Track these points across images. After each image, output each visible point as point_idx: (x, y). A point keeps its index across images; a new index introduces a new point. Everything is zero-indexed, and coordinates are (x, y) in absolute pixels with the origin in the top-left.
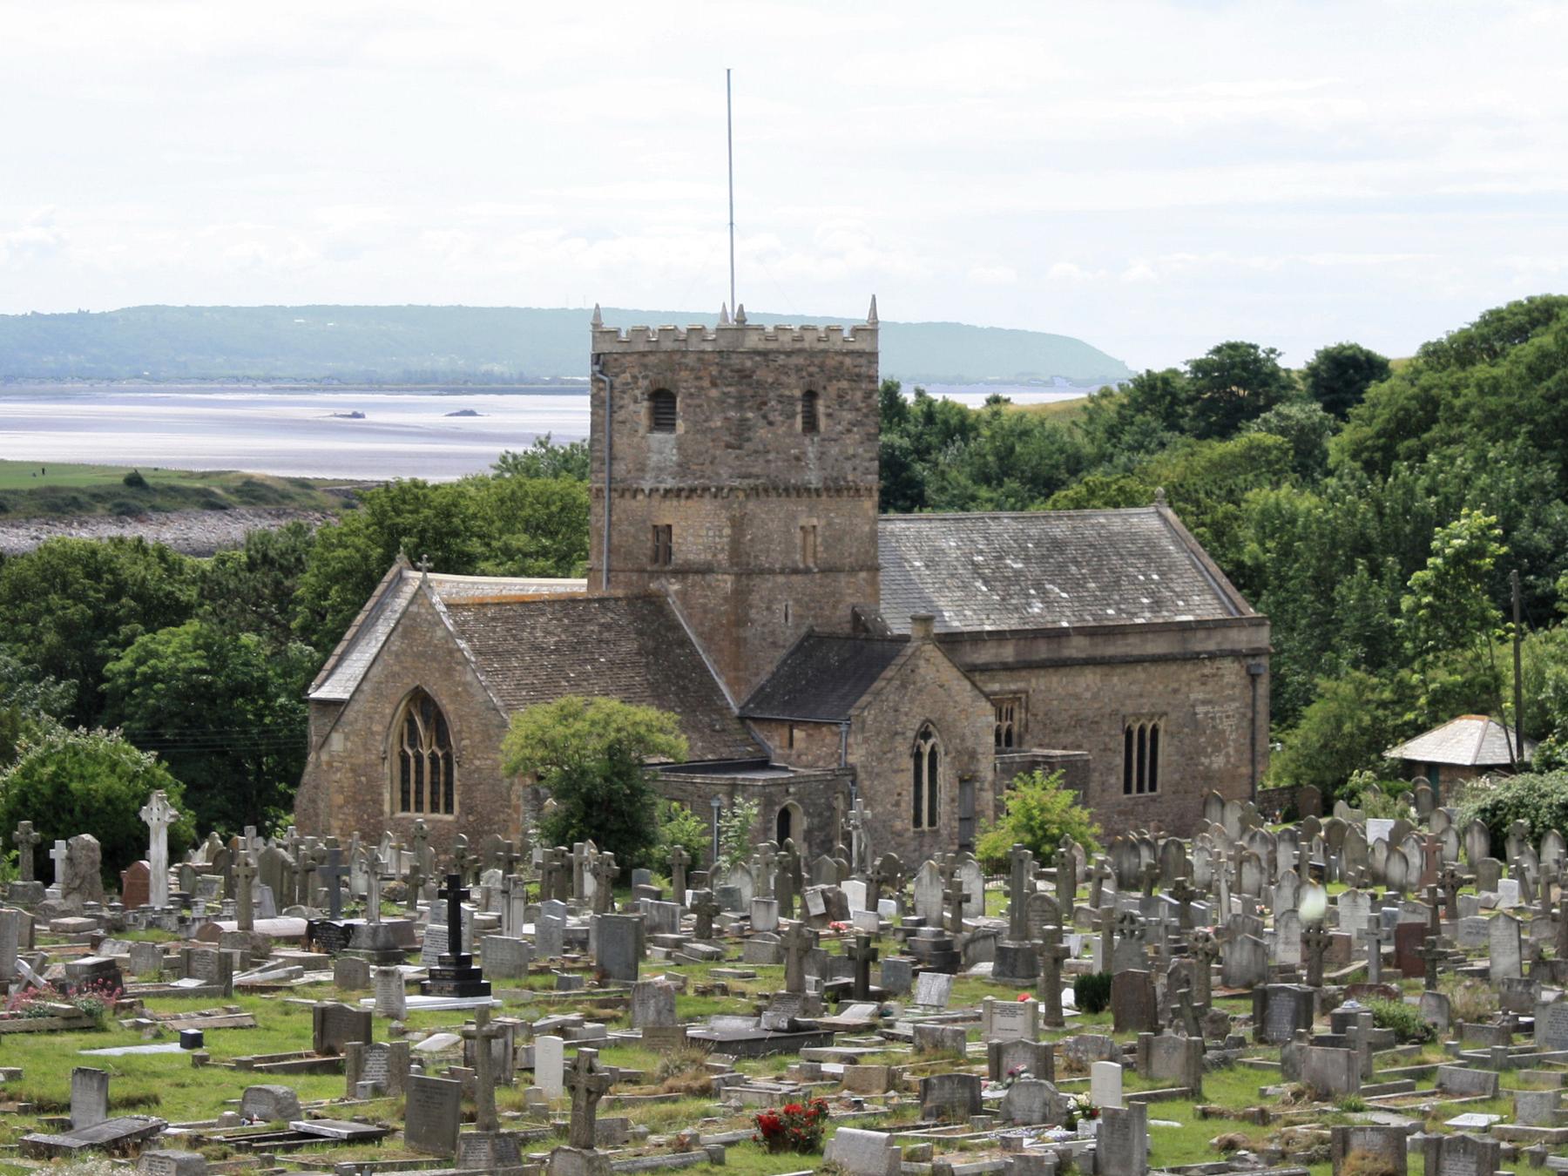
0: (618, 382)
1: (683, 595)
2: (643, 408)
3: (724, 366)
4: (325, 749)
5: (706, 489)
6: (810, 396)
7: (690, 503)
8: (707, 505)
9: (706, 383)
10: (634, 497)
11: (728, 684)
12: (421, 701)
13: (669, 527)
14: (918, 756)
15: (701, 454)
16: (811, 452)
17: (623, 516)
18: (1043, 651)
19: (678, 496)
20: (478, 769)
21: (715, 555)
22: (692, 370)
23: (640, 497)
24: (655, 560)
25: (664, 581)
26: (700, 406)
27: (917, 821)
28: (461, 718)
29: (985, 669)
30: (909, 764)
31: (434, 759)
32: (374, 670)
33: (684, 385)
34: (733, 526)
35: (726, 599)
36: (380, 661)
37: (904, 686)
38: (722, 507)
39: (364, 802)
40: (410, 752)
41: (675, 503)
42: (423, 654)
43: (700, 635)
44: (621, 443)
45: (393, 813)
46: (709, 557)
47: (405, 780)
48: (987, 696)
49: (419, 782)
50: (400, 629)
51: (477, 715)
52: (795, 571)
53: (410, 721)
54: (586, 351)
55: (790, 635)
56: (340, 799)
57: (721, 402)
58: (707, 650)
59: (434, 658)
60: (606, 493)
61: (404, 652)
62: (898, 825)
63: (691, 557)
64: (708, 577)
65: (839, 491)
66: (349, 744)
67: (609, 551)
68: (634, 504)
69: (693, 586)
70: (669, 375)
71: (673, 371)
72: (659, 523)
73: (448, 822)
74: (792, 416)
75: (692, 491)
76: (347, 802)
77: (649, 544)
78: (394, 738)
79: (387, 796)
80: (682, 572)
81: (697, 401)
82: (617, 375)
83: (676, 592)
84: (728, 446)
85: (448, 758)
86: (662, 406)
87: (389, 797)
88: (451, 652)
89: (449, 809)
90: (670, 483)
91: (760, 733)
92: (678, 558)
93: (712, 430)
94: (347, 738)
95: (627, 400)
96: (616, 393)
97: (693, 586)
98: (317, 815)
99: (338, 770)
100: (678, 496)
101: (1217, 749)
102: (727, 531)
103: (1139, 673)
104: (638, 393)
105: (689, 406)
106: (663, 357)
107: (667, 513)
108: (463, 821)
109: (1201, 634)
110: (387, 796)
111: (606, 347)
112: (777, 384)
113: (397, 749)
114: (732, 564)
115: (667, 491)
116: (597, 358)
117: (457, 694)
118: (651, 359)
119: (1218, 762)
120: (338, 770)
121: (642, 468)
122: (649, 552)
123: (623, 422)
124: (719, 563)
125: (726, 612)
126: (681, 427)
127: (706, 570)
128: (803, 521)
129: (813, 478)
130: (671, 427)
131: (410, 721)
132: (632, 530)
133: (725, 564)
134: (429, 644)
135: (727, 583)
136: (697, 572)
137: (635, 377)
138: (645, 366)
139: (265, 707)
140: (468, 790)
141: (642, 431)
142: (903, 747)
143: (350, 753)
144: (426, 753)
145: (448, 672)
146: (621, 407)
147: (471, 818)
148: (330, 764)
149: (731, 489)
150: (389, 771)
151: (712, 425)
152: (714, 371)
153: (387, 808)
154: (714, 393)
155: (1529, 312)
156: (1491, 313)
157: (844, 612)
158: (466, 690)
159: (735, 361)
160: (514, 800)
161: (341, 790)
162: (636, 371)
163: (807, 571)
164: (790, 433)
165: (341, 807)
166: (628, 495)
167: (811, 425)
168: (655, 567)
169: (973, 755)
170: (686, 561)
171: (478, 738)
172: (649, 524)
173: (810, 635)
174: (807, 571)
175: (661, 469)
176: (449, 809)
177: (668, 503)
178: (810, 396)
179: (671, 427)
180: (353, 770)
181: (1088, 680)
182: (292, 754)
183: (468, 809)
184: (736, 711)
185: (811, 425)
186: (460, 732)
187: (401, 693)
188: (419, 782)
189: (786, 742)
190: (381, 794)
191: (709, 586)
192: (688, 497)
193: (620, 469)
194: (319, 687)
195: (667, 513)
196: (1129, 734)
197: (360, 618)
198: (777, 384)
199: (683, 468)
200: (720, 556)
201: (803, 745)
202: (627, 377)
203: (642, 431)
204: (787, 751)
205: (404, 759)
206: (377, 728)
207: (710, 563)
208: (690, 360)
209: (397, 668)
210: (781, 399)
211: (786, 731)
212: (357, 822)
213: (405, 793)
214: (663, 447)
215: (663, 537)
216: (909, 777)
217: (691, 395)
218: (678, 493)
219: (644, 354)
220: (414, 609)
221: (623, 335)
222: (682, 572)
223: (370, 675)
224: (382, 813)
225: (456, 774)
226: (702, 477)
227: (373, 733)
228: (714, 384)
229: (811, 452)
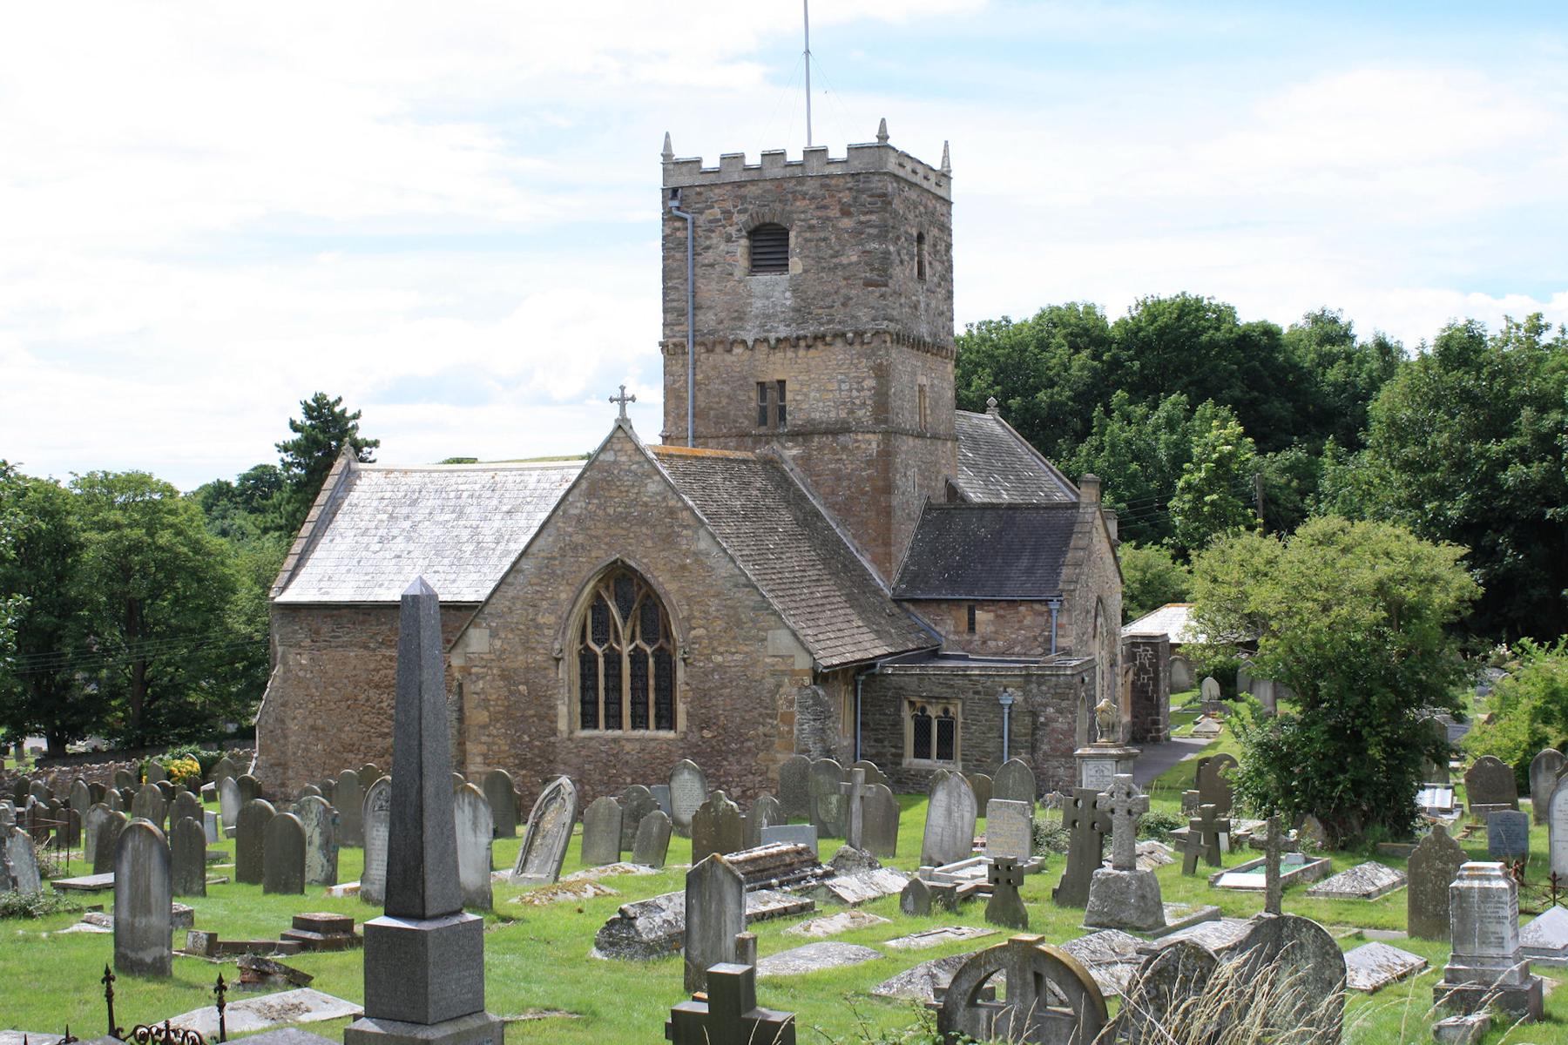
0: (701, 220)
1: (805, 461)
2: (741, 247)
3: (863, 191)
4: (459, 650)
7: (812, 352)
8: (839, 352)
9: (834, 212)
10: (729, 351)
11: (873, 561)
12: (622, 580)
13: (782, 384)
15: (828, 295)
17: (712, 373)
19: (796, 346)
20: (719, 667)
21: (851, 412)
22: (813, 198)
23: (738, 350)
24: (763, 420)
25: (776, 446)
26: (824, 240)
28: (689, 600)
31: (638, 658)
32: (540, 542)
34: (877, 377)
35: (870, 463)
36: (551, 529)
38: (860, 356)
39: (524, 719)
40: (599, 650)
41: (790, 354)
42: (625, 518)
43: (831, 506)
44: (710, 290)
45: (571, 732)
46: (843, 415)
50: (584, 485)
51: (717, 595)
54: (655, 179)
56: (483, 717)
57: (856, 233)
58: (843, 523)
59: (643, 522)
60: (689, 348)
61: (592, 516)
63: (816, 415)
64: (841, 438)
66: (498, 643)
67: (694, 415)
68: (729, 358)
69: (820, 449)
70: (778, 206)
71: (784, 201)
72: (766, 379)
73: (667, 741)
75: (819, 338)
76: (494, 719)
77: (753, 404)
78: (573, 633)
79: (562, 710)
80: (802, 434)
81: (822, 235)
82: (701, 212)
83: (794, 458)
84: (868, 283)
86: (768, 245)
87: (565, 711)
88: (672, 512)
89: (666, 719)
90: (783, 332)
91: (923, 617)
92: (795, 418)
93: (844, 267)
94: (494, 634)
95: (715, 239)
96: (700, 232)
97: (820, 449)
98: (285, 737)
99: (479, 677)
100: (796, 346)
102: (870, 383)
104: (732, 230)
105: (807, 240)
106: (769, 186)
107: (776, 367)
108: (694, 737)
111: (684, 180)
113: (577, 646)
114: (877, 421)
115: (778, 340)
116: (671, 193)
117: (684, 567)
118: (751, 190)
120: (479, 677)
121: (741, 317)
122: (755, 414)
123: (712, 266)
124: (859, 421)
125: (870, 478)
126: (796, 265)
127: (838, 430)
130: (783, 266)
131: (598, 607)
132: (727, 388)
133: (868, 421)
134: (634, 503)
136: (826, 433)
137: (727, 214)
138: (743, 198)
140: (702, 696)
141: (738, 274)
143: (500, 655)
144: (626, 649)
145: (669, 540)
146: (708, 248)
147: (707, 734)
148: (466, 670)
149: (877, 333)
150: (568, 674)
151: (845, 261)
152: (846, 197)
153: (562, 725)
154: (846, 223)
156: (138, 482)
158: (702, 565)
159: (876, 183)
160: (782, 706)
161: (485, 703)
162: (729, 205)
165: (484, 727)
166: (719, 349)
168: (763, 430)
170: (810, 421)
171: (719, 625)
172: (752, 381)
175: (768, 317)
176: (666, 719)
177: (780, 355)
179: (783, 266)
180: (503, 677)
182: (248, 668)
183: (701, 721)
184: (888, 593)
186: (688, 619)
187: (586, 572)
189: (964, 625)
190: (553, 707)
191: (844, 448)
192: (808, 347)
194: (283, 589)
197: (314, 513)
199: (801, 313)
200: (860, 413)
201: (991, 628)
203: (738, 274)
204: (966, 637)
205: (587, 659)
206: (546, 619)
207: (844, 421)
208: (811, 187)
209: (579, 539)
211: (964, 614)
212: (513, 745)
214: (772, 292)
215: (772, 395)
217: (811, 228)
218: (794, 343)
219: (740, 185)
220: (608, 457)
221: (706, 165)
222: (802, 434)
223: (534, 549)
224: (554, 732)
225: (681, 674)
226: (829, 322)
227: (538, 627)
228: (846, 213)
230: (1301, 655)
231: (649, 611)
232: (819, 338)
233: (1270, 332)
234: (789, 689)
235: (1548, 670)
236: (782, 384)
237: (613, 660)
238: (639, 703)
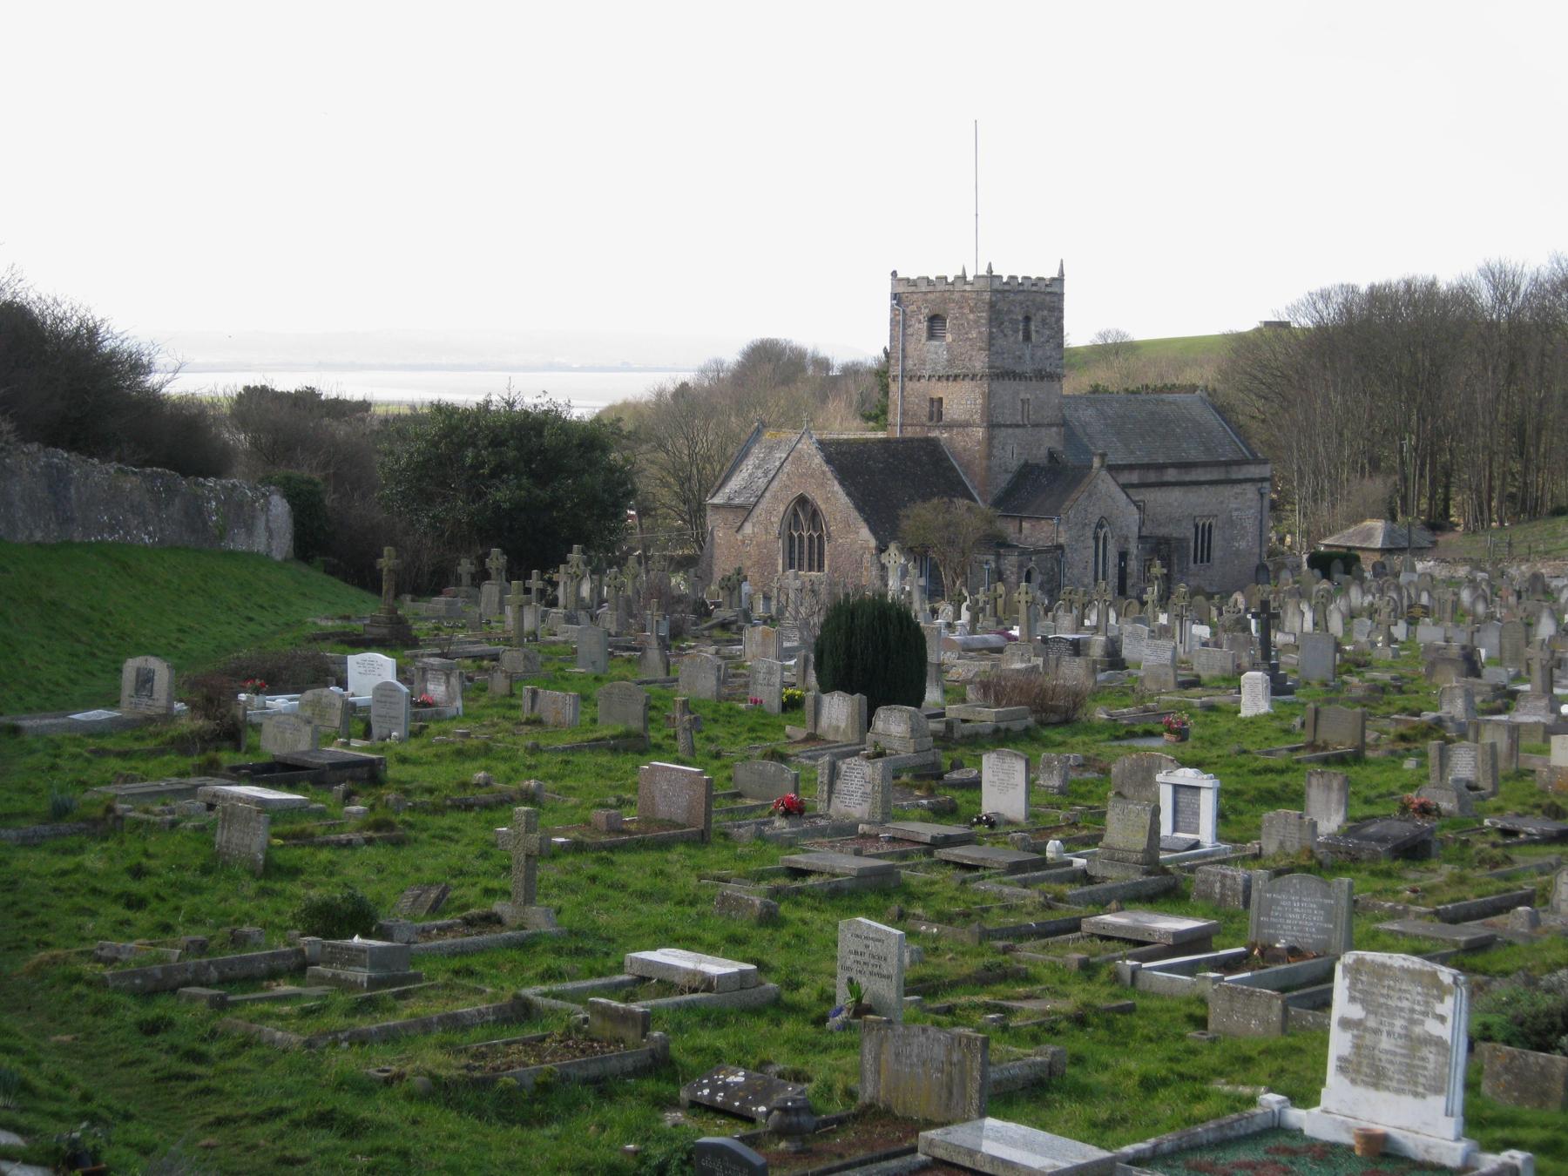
5: (965, 376)
6: (1027, 319)
9: (966, 311)
12: (802, 501)
13: (941, 400)
14: (1096, 539)
16: (1028, 353)
18: (1152, 477)
20: (842, 545)
24: (931, 419)
27: (1096, 580)
29: (1133, 486)
30: (1092, 543)
31: (811, 538)
33: (952, 311)
37: (1090, 495)
47: (791, 552)
48: (1135, 503)
49: (801, 553)
52: (1018, 426)
53: (796, 515)
55: (1014, 464)
57: (976, 322)
62: (1086, 581)
65: (1042, 378)
74: (1017, 331)
75: (956, 377)
80: (950, 426)
85: (820, 537)
89: (821, 568)
92: (946, 418)
101: (1243, 537)
103: (1203, 490)
107: (938, 390)
109: (1235, 468)
110: (780, 561)
111: (900, 290)
112: (1009, 312)
119: (1243, 545)
126: (949, 338)
127: (966, 425)
128: (1022, 396)
129: (1028, 367)
135: (979, 433)
139: (1476, 619)
142: (1089, 533)
154: (971, 316)
155: (497, 442)
157: (1043, 452)
163: (1024, 426)
164: (1016, 342)
167: (1027, 337)
169: (1126, 539)
173: (1026, 464)
174: (1024, 426)
178: (1027, 319)
181: (1176, 494)
183: (834, 570)
185: (1027, 337)
188: (801, 553)
193: (910, 363)
195: (938, 390)
196: (1197, 527)
198: (1009, 312)
202: (914, 308)
205: (791, 537)
208: (956, 296)
210: (1012, 321)
213: (791, 559)
216: (1092, 551)
222: (950, 426)
228: (972, 311)
229: (1028, 353)
230: (443, 725)
231: (815, 516)
232: (956, 377)
233: (684, 386)
234: (867, 556)
235: (131, 938)
236: (941, 400)
237: (800, 536)
238: (811, 559)
